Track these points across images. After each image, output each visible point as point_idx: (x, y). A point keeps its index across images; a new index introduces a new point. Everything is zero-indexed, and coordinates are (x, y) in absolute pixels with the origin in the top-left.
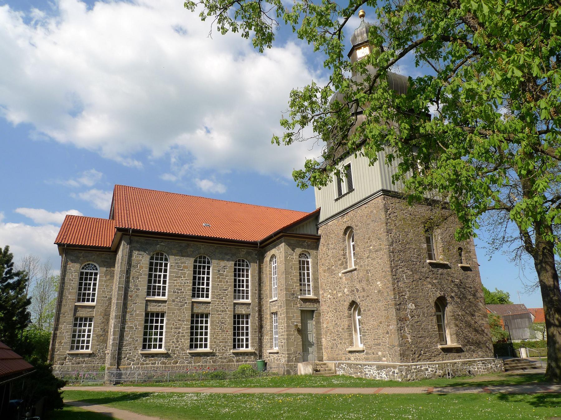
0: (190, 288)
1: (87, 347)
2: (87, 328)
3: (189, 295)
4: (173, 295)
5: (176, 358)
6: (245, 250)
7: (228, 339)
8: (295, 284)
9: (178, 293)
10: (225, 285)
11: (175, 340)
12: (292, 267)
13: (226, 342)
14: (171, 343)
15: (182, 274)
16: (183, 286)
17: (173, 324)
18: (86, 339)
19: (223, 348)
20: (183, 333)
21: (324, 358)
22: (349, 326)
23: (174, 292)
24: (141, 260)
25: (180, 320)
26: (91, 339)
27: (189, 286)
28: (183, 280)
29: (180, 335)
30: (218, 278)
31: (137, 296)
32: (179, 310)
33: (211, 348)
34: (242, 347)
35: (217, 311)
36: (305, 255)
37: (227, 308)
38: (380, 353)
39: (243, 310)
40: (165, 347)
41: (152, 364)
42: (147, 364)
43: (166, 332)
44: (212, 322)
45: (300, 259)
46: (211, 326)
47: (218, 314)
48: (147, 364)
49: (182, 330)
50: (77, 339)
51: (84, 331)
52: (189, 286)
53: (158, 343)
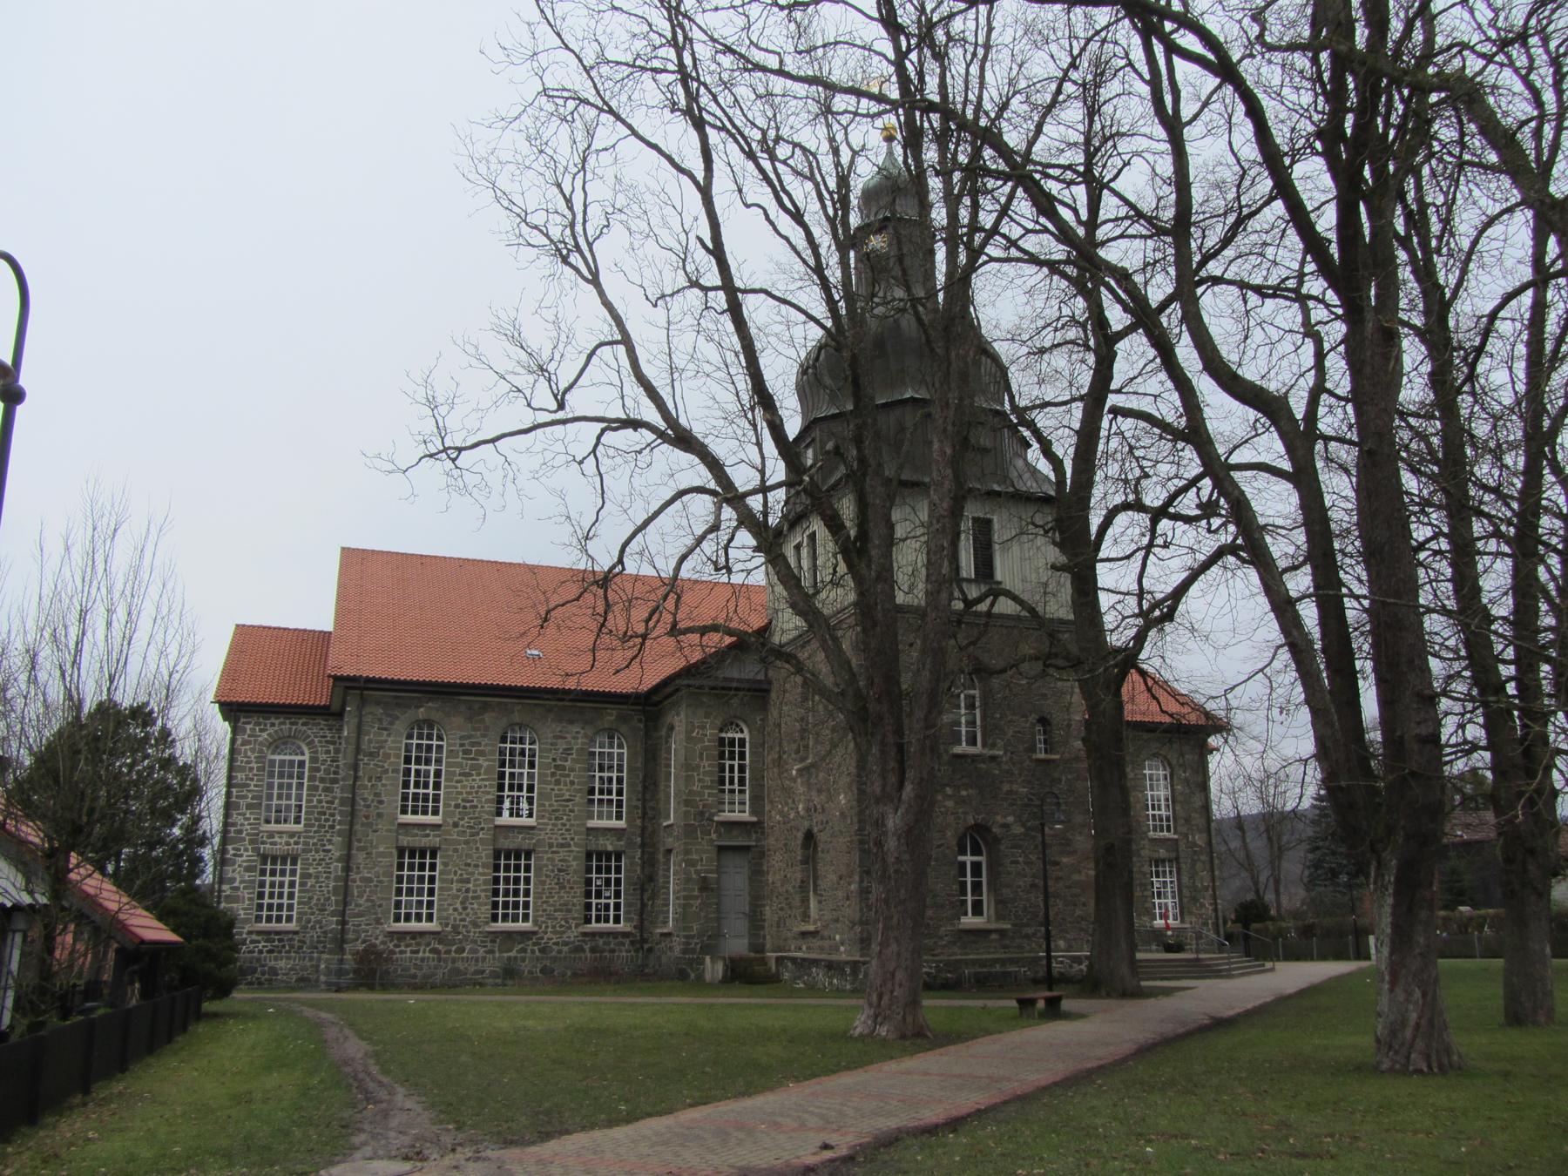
0: (490, 797)
1: (289, 919)
2: (287, 879)
3: (488, 813)
4: (454, 813)
5: (461, 941)
6: (614, 712)
7: (574, 905)
8: (707, 791)
9: (465, 807)
10: (568, 790)
11: (458, 906)
12: (701, 754)
13: (569, 911)
14: (451, 911)
15: (473, 767)
16: (477, 793)
17: (455, 873)
18: (285, 901)
19: (563, 923)
20: (475, 891)
21: (768, 946)
22: (802, 882)
23: (457, 806)
24: (386, 741)
25: (469, 865)
26: (435, 898)
27: (489, 793)
28: (476, 780)
29: (470, 895)
30: (553, 774)
31: (380, 815)
32: (467, 842)
33: (535, 922)
34: (607, 921)
35: (551, 846)
36: (738, 726)
37: (572, 839)
38: (838, 937)
39: (608, 843)
40: (438, 919)
41: (412, 952)
42: (401, 952)
43: (440, 888)
44: (539, 869)
45: (723, 735)
46: (535, 876)
47: (553, 852)
48: (401, 952)
49: (475, 886)
50: (266, 901)
51: (282, 885)
52: (489, 793)
53: (521, 911)
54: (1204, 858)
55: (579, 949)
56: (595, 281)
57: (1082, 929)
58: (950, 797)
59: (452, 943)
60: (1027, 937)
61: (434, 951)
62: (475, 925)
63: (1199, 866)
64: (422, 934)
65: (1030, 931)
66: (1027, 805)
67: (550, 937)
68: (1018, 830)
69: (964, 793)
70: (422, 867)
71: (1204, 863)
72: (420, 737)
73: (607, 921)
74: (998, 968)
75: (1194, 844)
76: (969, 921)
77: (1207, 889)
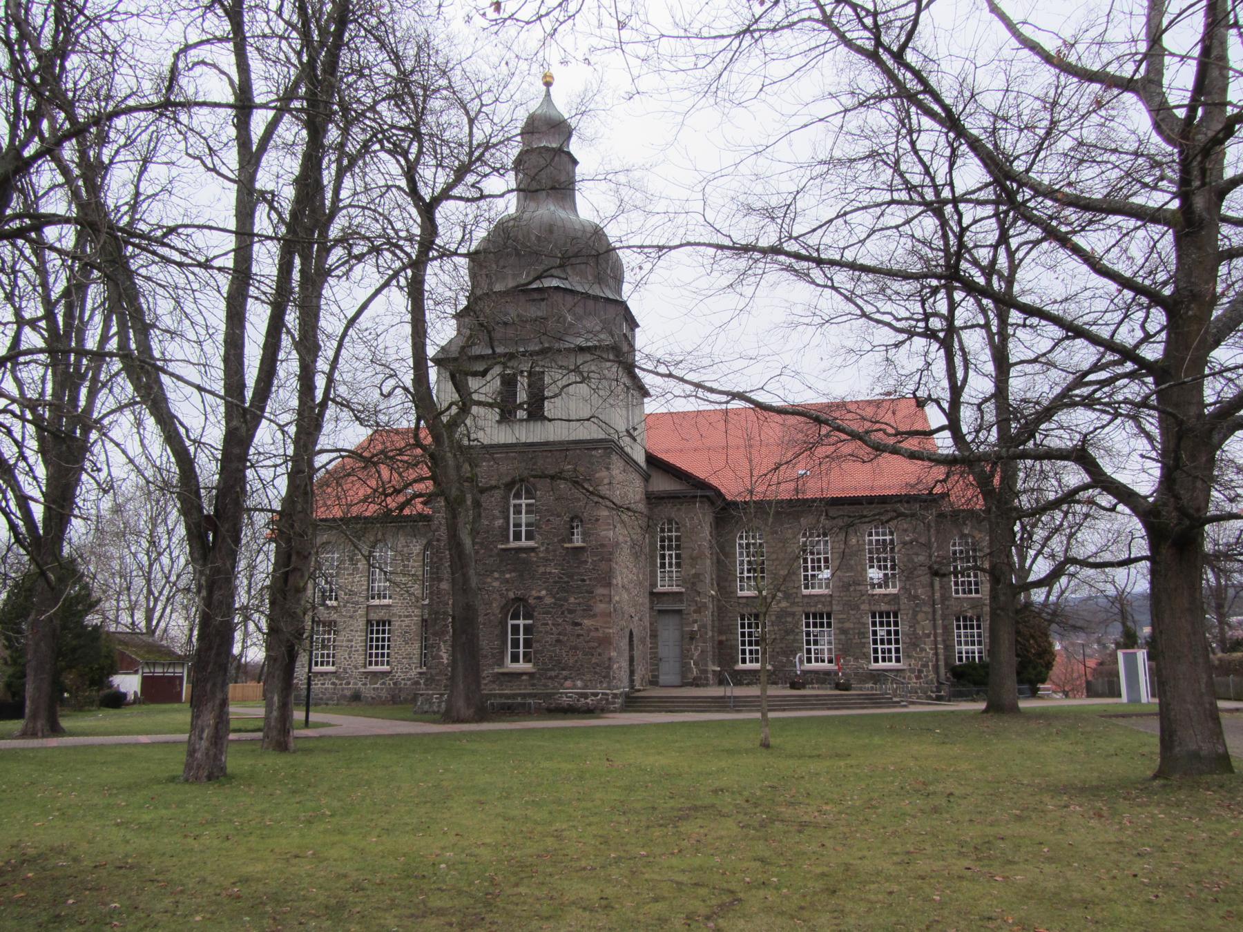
54: (927, 609)
55: (417, 683)
56: (671, 248)
57: (596, 673)
58: (497, 579)
59: (343, 679)
60: (551, 678)
61: (333, 684)
62: (356, 668)
63: (920, 616)
64: (326, 673)
65: (553, 674)
66: (556, 582)
67: (399, 675)
68: (549, 600)
69: (508, 576)
70: (889, 624)
71: (925, 613)
72: (877, 534)
73: (890, 660)
74: (519, 700)
75: (916, 597)
76: (512, 667)
77: (928, 636)
